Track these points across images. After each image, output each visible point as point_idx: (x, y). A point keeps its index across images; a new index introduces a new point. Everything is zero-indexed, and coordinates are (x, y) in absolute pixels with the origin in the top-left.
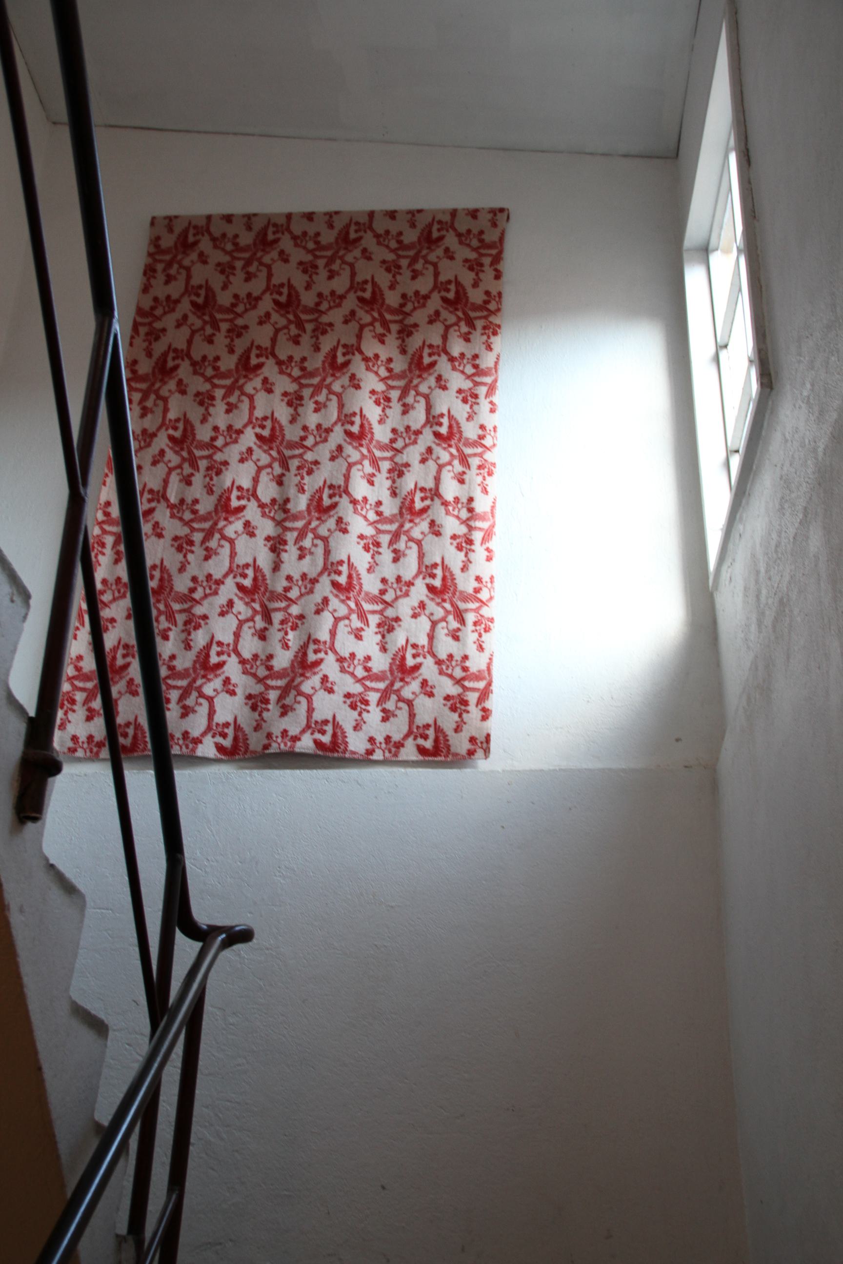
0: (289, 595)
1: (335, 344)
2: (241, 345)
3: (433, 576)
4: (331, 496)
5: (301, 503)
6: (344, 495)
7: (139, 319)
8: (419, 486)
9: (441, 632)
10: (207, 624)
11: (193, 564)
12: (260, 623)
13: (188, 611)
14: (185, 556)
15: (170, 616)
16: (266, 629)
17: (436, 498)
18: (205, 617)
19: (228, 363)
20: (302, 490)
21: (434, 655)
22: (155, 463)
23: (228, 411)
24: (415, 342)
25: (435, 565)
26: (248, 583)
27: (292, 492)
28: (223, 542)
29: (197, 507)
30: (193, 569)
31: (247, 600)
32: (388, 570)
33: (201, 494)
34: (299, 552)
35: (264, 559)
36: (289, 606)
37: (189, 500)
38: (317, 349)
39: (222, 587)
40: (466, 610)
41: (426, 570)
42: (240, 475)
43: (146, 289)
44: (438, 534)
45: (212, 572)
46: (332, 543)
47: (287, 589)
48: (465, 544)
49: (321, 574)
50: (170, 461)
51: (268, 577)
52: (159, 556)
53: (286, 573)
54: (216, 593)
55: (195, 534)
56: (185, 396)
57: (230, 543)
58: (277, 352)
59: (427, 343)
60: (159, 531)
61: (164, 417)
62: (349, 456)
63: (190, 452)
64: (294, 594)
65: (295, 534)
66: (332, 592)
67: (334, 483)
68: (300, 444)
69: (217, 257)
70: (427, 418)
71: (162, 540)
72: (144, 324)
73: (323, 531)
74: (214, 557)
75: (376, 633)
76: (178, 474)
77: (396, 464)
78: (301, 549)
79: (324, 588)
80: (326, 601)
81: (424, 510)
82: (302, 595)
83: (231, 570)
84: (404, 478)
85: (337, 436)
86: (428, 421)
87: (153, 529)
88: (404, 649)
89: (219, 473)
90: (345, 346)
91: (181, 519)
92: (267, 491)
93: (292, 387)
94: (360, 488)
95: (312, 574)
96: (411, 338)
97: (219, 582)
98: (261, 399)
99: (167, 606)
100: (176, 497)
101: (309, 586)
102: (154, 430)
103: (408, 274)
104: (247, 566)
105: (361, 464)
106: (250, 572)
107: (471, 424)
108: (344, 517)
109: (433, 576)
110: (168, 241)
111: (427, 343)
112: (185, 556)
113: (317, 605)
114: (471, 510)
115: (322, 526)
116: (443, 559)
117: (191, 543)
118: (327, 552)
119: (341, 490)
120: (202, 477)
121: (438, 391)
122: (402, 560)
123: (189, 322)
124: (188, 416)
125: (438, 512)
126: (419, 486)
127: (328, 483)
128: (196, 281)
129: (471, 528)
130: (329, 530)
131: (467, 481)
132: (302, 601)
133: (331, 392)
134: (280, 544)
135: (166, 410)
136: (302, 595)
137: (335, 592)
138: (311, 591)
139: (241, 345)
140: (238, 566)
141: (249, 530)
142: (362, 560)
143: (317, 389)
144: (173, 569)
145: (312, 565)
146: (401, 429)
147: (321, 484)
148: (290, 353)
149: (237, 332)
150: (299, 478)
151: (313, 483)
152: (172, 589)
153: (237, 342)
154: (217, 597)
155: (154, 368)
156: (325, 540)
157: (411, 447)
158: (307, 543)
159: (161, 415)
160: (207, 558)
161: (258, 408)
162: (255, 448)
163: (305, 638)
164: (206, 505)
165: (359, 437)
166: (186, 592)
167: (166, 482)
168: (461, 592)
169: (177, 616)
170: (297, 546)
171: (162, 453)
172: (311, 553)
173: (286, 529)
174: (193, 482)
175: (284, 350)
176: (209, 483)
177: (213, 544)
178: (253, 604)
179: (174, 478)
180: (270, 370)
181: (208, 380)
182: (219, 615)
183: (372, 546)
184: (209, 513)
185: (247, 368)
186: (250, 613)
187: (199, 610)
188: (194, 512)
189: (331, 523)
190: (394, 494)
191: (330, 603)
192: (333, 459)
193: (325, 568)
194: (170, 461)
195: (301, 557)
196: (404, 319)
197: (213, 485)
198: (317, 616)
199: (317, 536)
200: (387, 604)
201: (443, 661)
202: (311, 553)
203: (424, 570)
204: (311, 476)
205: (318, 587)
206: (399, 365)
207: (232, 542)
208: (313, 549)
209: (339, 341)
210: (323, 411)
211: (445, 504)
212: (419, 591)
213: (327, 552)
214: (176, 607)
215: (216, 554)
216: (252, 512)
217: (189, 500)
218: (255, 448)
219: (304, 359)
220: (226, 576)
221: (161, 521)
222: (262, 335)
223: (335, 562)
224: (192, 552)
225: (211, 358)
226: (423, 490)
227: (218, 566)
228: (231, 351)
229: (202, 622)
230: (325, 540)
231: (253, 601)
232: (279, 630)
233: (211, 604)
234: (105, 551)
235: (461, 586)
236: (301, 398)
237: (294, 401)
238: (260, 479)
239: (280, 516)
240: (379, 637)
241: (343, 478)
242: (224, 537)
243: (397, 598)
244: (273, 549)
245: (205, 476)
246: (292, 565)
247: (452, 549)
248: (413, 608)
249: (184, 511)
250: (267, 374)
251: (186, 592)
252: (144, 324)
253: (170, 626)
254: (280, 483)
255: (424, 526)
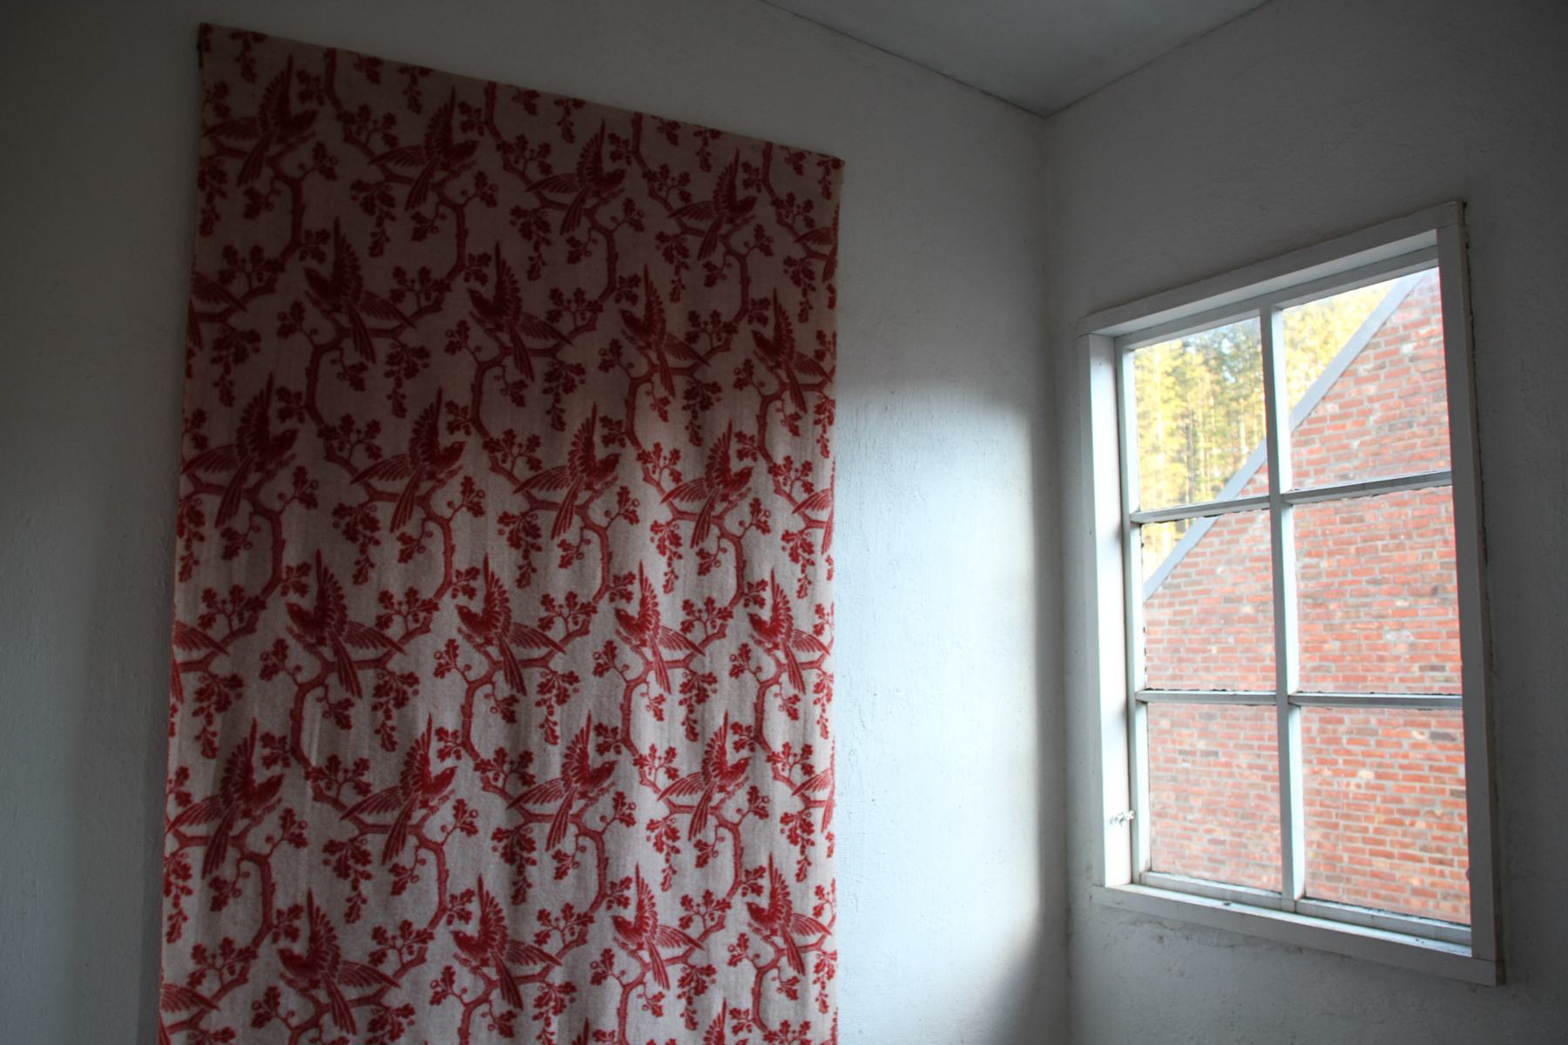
0: (546, 948)
1: (589, 415)
2: (417, 394)
3: (758, 890)
4: (602, 749)
5: (551, 764)
6: (624, 750)
7: (200, 306)
8: (731, 721)
9: (772, 985)
10: (412, 1023)
11: (372, 903)
12: (499, 1005)
13: (374, 1000)
14: (355, 887)
15: (342, 1015)
16: (511, 1015)
17: (757, 746)
18: (408, 1011)
19: (396, 439)
20: (551, 738)
21: (762, 1026)
22: (268, 673)
23: (405, 557)
24: (717, 420)
25: (759, 872)
26: (472, 929)
27: (535, 739)
28: (424, 853)
29: (367, 777)
30: (373, 915)
31: (474, 963)
32: (691, 882)
33: (370, 748)
34: (555, 864)
35: (496, 877)
36: (547, 970)
37: (348, 762)
38: (559, 424)
39: (431, 945)
40: (806, 948)
41: (748, 879)
42: (438, 704)
43: (207, 226)
44: (762, 814)
45: (410, 917)
46: (610, 846)
47: (542, 938)
48: (801, 830)
49: (595, 905)
50: (298, 668)
51: (504, 913)
52: (303, 886)
53: (538, 908)
54: (421, 959)
55: (369, 837)
56: (313, 512)
57: (435, 851)
58: (485, 418)
59: (736, 430)
60: (295, 830)
61: (277, 560)
62: (626, 667)
63: (339, 651)
64: (553, 946)
65: (547, 827)
66: (615, 939)
67: (605, 723)
68: (536, 635)
69: (354, 166)
70: (739, 586)
71: (304, 851)
72: (211, 317)
73: (593, 821)
74: (410, 885)
75: (679, 997)
76: (319, 700)
77: (693, 673)
78: (559, 856)
79: (602, 933)
80: (608, 956)
81: (741, 767)
82: (567, 947)
83: (442, 909)
84: (707, 705)
85: (603, 625)
86: (740, 593)
87: (284, 827)
88: (720, 1021)
89: (401, 701)
90: (606, 421)
91: (336, 803)
92: (489, 735)
93: (517, 505)
94: (650, 733)
95: (581, 908)
96: (708, 413)
97: (425, 937)
98: (294, 521)
99: (333, 993)
100: (319, 752)
101: (577, 929)
102: (258, 591)
103: (700, 272)
104: (468, 895)
105: (645, 681)
106: (474, 907)
107: (804, 603)
108: (626, 793)
109: (758, 890)
110: (246, 102)
111: (736, 430)
112: (355, 887)
113: (594, 965)
114: (808, 769)
115: (591, 809)
116: (771, 859)
117: (364, 857)
118: (603, 863)
119: (617, 737)
120: (369, 709)
121: (754, 533)
122: (711, 861)
123: (307, 324)
124: (325, 561)
125: (762, 772)
126: (731, 721)
127: (595, 721)
128: (314, 221)
129: (809, 803)
130: (603, 818)
131: (801, 714)
132: (568, 958)
133: (588, 525)
134: (523, 848)
135: (278, 546)
136: (567, 947)
137: (621, 938)
138: (582, 940)
139: (417, 394)
140: (453, 897)
141: (465, 820)
142: (652, 865)
143: (564, 514)
144: (334, 912)
145: (577, 889)
146: (700, 604)
147: (583, 724)
148: (508, 426)
149: (409, 362)
150: (544, 709)
151: (571, 718)
152: (337, 956)
153: (409, 387)
154: (423, 967)
155: (241, 431)
156: (597, 837)
157: (717, 643)
158: (567, 845)
159: (269, 555)
160: (398, 889)
161: (458, 548)
162: (460, 640)
163: (580, 1027)
164: (382, 775)
165: (637, 626)
166: (365, 961)
167: (296, 717)
168: (799, 916)
169: (356, 1013)
170: (552, 852)
171: (280, 648)
172: (577, 864)
173: (531, 817)
174: (353, 721)
175: (500, 417)
176: (383, 725)
177: (405, 858)
178: (485, 970)
179: (313, 710)
180: (473, 462)
181: (361, 477)
182: (432, 1003)
183: (665, 837)
184: (391, 791)
185: (433, 457)
186: (481, 987)
187: (395, 999)
188: (363, 789)
189: (605, 804)
190: (692, 734)
191: (615, 960)
192: (600, 671)
193: (601, 895)
194: (298, 668)
195: (560, 874)
196: (200, 1016)
197: (393, 729)
198: (595, 987)
199: (584, 832)
200: (694, 944)
201: (775, 1034)
202: (577, 864)
203: (743, 878)
204: (565, 706)
205: (593, 929)
206: (691, 469)
207: (438, 849)
208: (578, 857)
209: (595, 410)
210: (576, 563)
211: (772, 758)
212: (738, 918)
213: (603, 863)
214: (351, 993)
215: (415, 878)
216: (466, 783)
217: (348, 762)
218: (460, 640)
219: (534, 442)
220: (434, 922)
221: (297, 810)
222: (453, 376)
223: (617, 881)
224: (368, 877)
225: (361, 424)
226: (737, 727)
227: (419, 904)
228: (400, 411)
229: (404, 1021)
230: (597, 837)
231: (485, 963)
232: (536, 1018)
233: (415, 983)
234: (190, 884)
235: (797, 908)
236: (534, 532)
237: (524, 535)
238: (475, 710)
239: (516, 789)
240: (683, 1001)
241: (619, 713)
242: (424, 843)
243: (706, 933)
244: (509, 856)
245: (375, 708)
246: (547, 891)
247: (783, 840)
248: (731, 949)
249: (340, 785)
250: (469, 470)
251: (365, 961)
252: (211, 317)
253: (344, 1034)
254: (510, 717)
255: (741, 798)
